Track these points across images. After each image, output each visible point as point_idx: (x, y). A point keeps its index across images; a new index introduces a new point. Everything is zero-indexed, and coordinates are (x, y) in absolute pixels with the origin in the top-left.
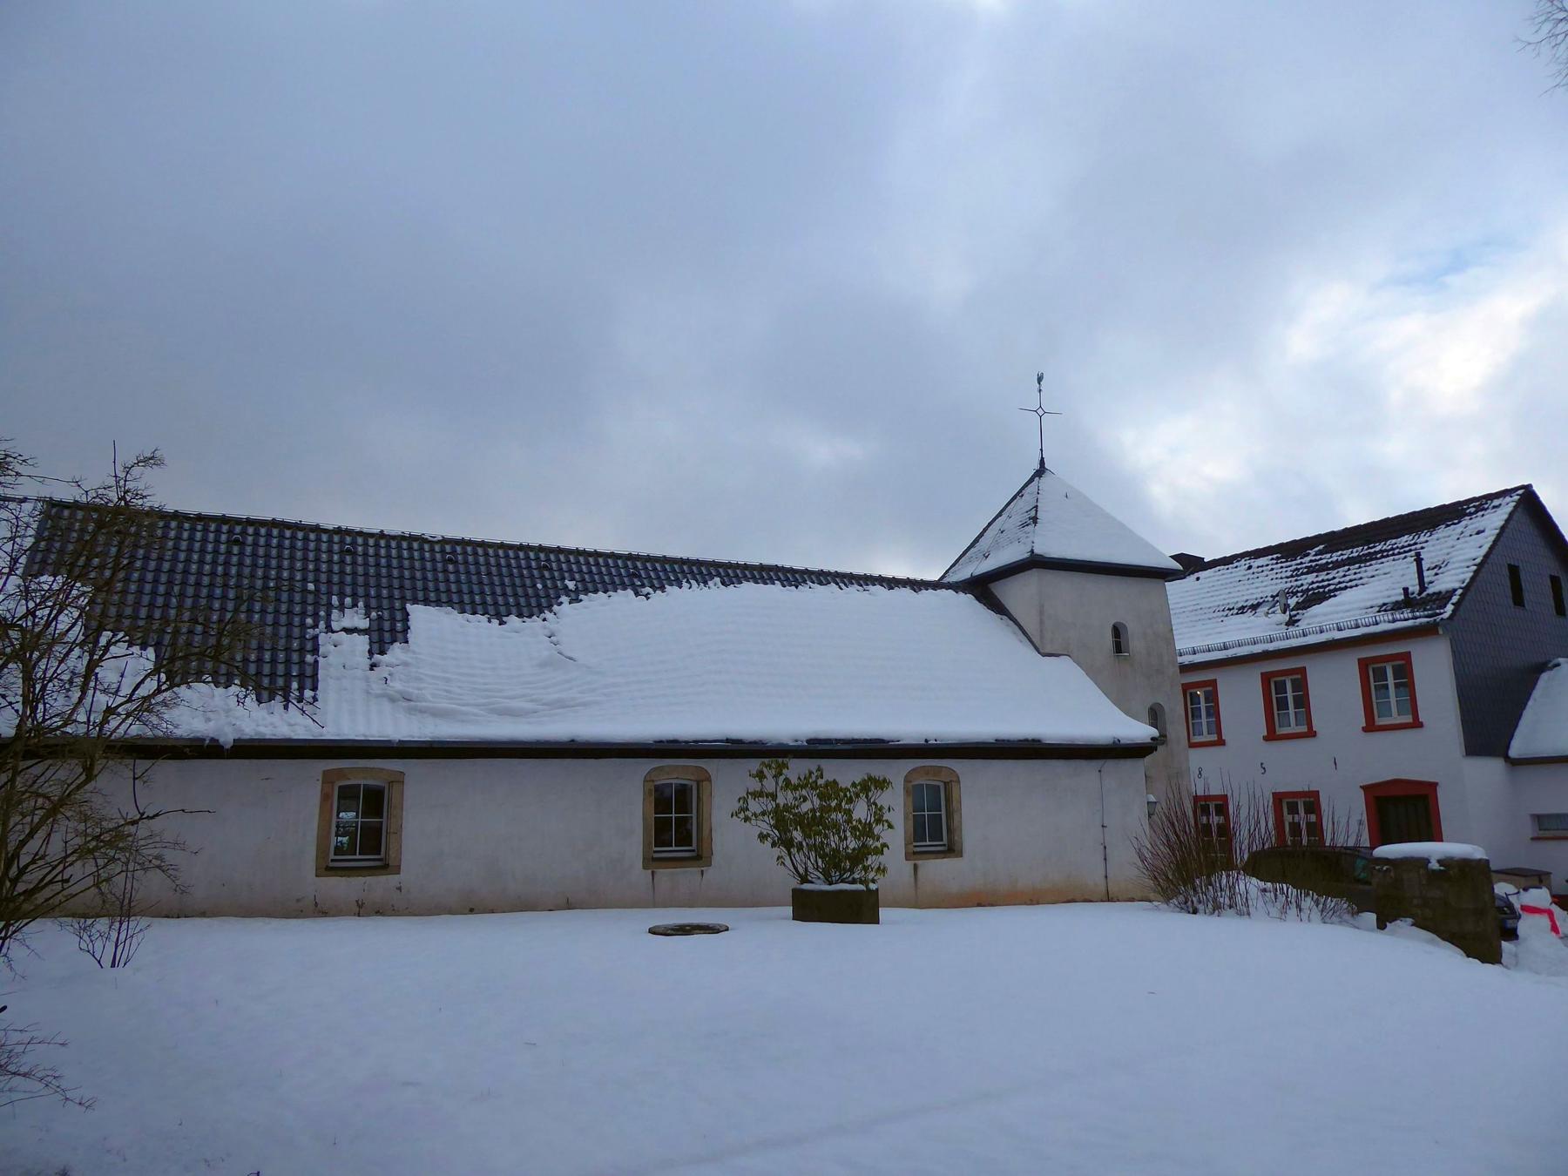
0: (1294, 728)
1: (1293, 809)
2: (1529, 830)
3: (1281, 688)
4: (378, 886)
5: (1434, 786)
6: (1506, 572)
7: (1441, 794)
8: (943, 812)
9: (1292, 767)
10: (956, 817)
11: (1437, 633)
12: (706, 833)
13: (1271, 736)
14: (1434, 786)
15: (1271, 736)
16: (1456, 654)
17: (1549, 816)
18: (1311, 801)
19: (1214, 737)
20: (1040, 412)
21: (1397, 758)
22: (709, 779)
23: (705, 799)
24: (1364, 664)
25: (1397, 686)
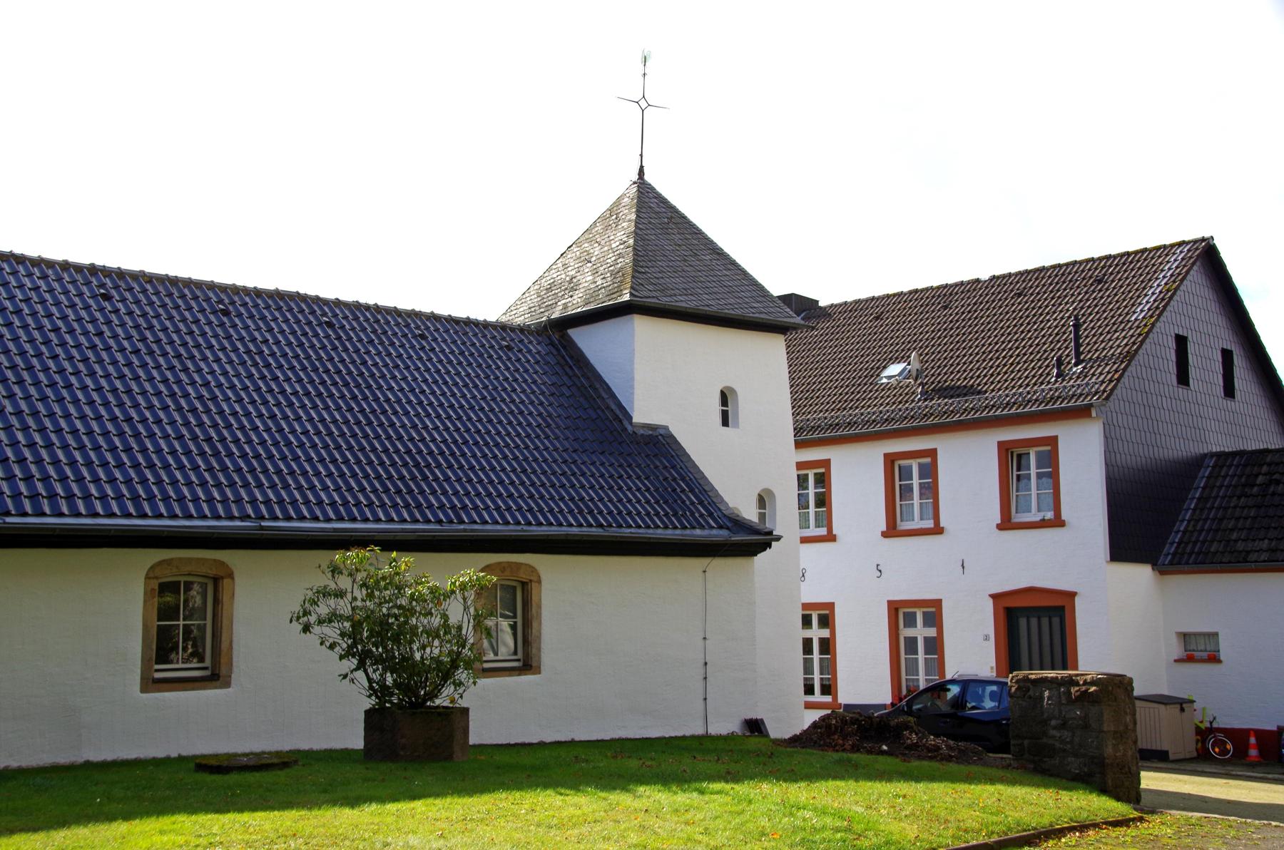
0: (916, 524)
1: (910, 621)
2: (1177, 650)
3: (906, 474)
4: (218, 683)
5: (1072, 595)
6: (1172, 344)
7: (1079, 603)
8: (209, 622)
9: (915, 569)
10: (535, 625)
11: (1089, 415)
12: (224, 646)
13: (892, 531)
14: (1072, 595)
15: (892, 531)
16: (1107, 438)
17: (1195, 634)
18: (933, 611)
19: (823, 531)
20: (643, 104)
21: (1033, 562)
22: (231, 575)
23: (226, 599)
24: (1005, 449)
25: (1039, 476)
